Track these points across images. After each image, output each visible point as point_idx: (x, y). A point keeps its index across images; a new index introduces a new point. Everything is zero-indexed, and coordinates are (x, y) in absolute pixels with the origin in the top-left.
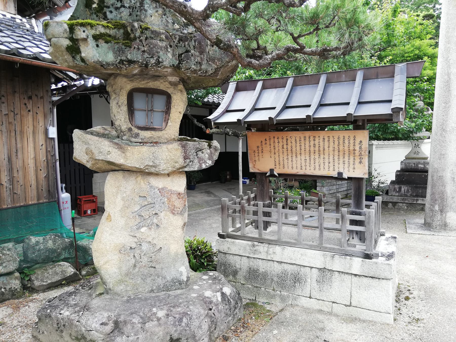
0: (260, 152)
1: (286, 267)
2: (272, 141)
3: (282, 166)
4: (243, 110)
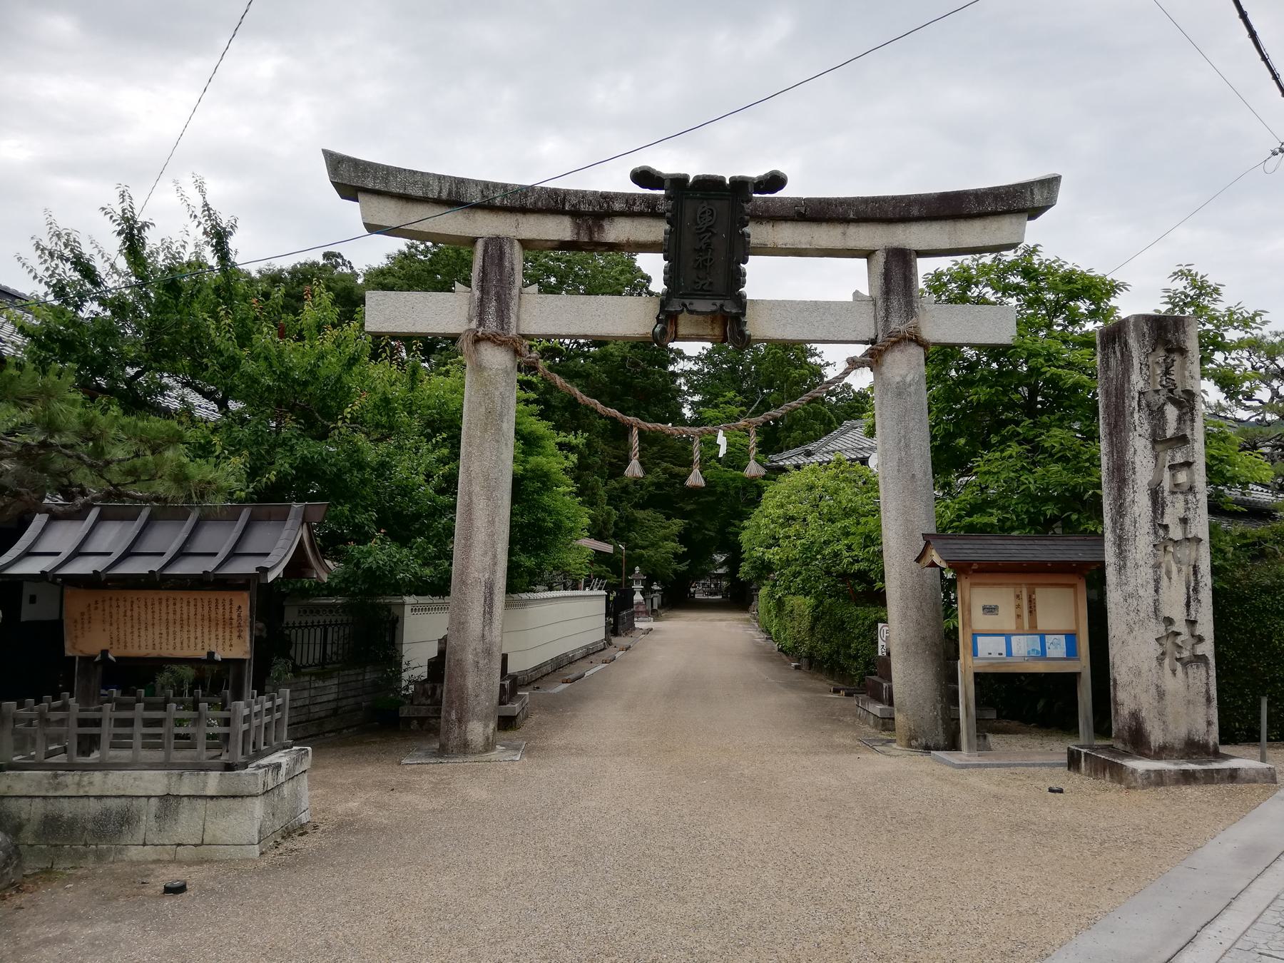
0: (86, 622)
1: (109, 802)
2: (107, 603)
3: (122, 644)
4: (57, 554)
